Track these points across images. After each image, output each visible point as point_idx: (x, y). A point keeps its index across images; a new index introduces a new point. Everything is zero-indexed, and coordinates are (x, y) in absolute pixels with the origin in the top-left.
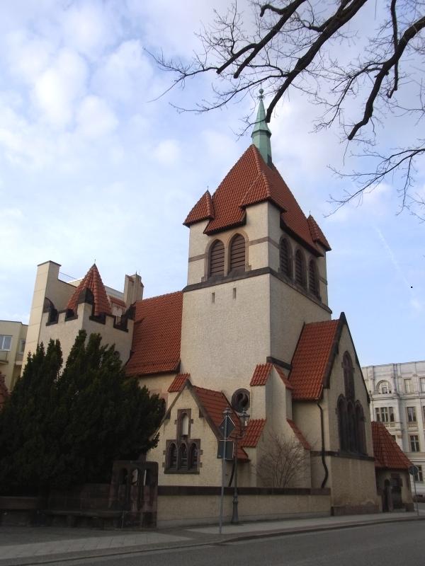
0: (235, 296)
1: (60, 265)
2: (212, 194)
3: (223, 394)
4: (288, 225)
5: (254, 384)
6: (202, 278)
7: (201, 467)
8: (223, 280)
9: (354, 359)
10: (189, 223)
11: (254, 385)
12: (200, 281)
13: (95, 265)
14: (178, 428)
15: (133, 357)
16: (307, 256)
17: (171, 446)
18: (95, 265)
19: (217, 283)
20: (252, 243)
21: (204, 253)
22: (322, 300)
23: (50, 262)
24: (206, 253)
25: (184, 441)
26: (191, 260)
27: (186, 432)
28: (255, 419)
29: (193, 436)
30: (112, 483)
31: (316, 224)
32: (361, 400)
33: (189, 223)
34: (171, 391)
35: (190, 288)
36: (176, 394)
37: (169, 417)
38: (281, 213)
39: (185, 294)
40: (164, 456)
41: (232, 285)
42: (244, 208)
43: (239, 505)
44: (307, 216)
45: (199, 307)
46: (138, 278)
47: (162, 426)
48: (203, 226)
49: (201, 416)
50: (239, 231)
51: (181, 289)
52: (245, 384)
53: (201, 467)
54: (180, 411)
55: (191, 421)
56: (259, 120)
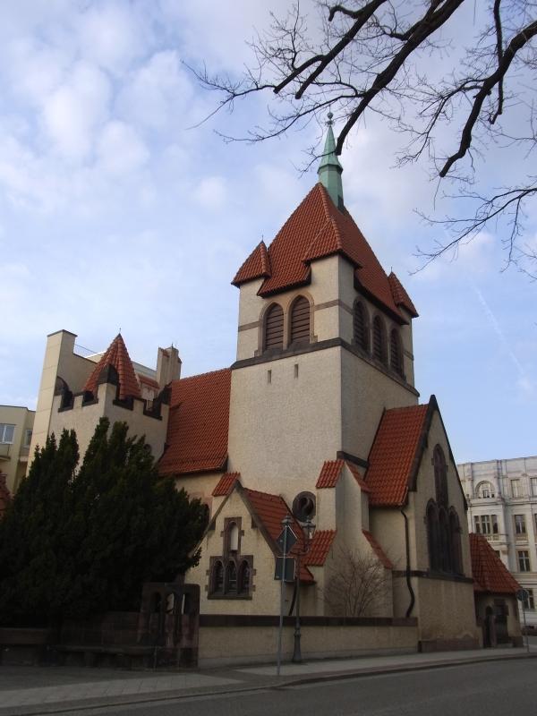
0: (297, 375)
1: (76, 336)
2: (268, 246)
3: (282, 498)
6: (256, 352)
8: (282, 354)
10: (238, 283)
15: (168, 451)
16: (388, 324)
17: (217, 564)
18: (119, 335)
19: (274, 358)
20: (319, 307)
22: (407, 379)
23: (64, 331)
25: (232, 559)
26: (241, 329)
27: (235, 547)
32: (456, 506)
33: (238, 283)
34: (216, 494)
35: (240, 364)
36: (222, 499)
37: (213, 527)
41: (293, 360)
42: (308, 263)
44: (388, 274)
49: (254, 526)
50: (302, 292)
51: (228, 366)
52: (310, 486)
54: (228, 520)
55: (242, 533)
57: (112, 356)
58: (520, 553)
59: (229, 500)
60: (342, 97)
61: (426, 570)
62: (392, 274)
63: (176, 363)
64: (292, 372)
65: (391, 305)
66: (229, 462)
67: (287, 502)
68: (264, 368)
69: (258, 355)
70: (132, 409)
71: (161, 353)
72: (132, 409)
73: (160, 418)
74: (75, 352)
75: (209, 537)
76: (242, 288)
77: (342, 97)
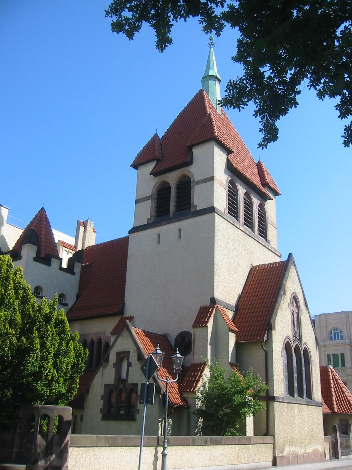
0: (180, 237)
2: (160, 137)
3: (166, 337)
4: (235, 165)
5: (194, 326)
6: (148, 219)
7: (138, 413)
8: (169, 221)
9: (312, 324)
10: (136, 166)
11: (196, 327)
12: (145, 222)
13: (43, 208)
14: (116, 372)
15: (79, 299)
16: (256, 202)
17: (109, 390)
18: (43, 208)
20: (198, 183)
21: (150, 194)
22: (271, 243)
24: (152, 194)
25: (121, 386)
26: (137, 201)
27: (124, 376)
28: (196, 363)
29: (131, 381)
30: (18, 430)
32: (308, 342)
33: (136, 166)
34: (113, 333)
36: (115, 336)
37: (107, 360)
38: (228, 155)
40: (102, 401)
43: (168, 457)
47: (101, 370)
48: (150, 167)
52: (188, 326)
53: (138, 413)
54: (119, 354)
55: (129, 365)
56: (219, 83)
58: (293, 306)
59: (120, 338)
60: (304, 89)
61: (235, 334)
65: (257, 182)
66: (125, 305)
67: (170, 340)
69: (150, 222)
70: (49, 265)
72: (49, 265)
73: (73, 273)
75: (105, 367)
77: (304, 89)
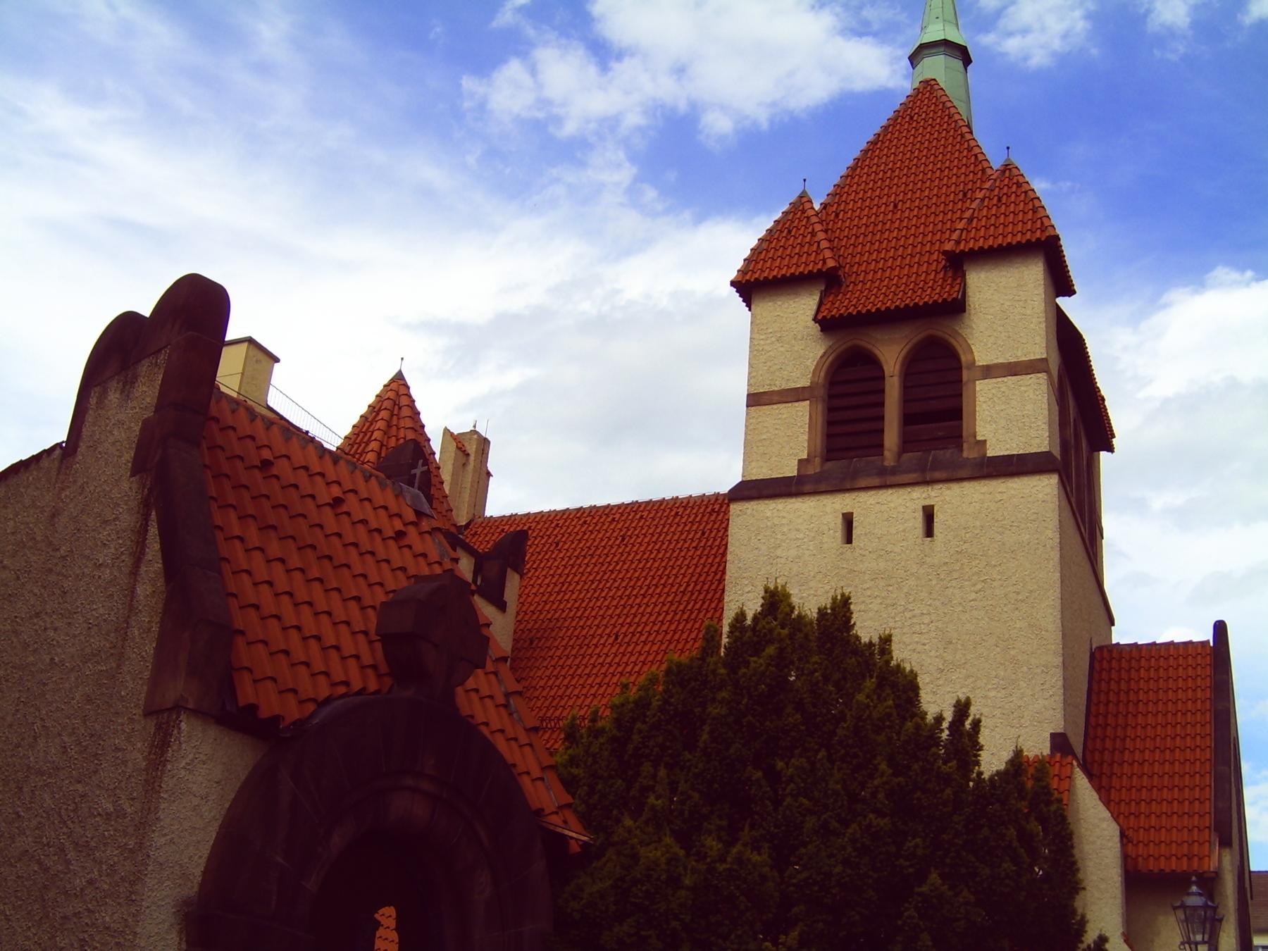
0: (929, 532)
1: (277, 360)
12: (791, 470)
13: (399, 379)
18: (399, 379)
19: (863, 483)
20: (989, 371)
23: (250, 341)
26: (755, 400)
31: (1110, 424)
35: (748, 491)
39: (735, 508)
41: (918, 497)
42: (957, 263)
44: (996, 162)
45: (793, 553)
46: (484, 443)
49: (969, 716)
50: (940, 329)
51: (724, 489)
57: (389, 426)
62: (1008, 168)
63: (485, 475)
64: (918, 522)
68: (828, 508)
69: (811, 471)
71: (452, 446)
74: (271, 404)
76: (759, 306)
